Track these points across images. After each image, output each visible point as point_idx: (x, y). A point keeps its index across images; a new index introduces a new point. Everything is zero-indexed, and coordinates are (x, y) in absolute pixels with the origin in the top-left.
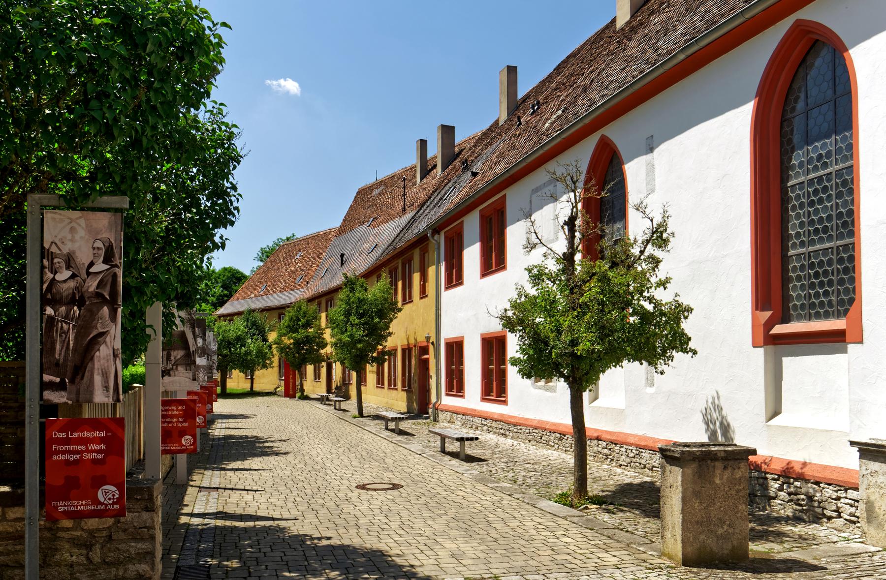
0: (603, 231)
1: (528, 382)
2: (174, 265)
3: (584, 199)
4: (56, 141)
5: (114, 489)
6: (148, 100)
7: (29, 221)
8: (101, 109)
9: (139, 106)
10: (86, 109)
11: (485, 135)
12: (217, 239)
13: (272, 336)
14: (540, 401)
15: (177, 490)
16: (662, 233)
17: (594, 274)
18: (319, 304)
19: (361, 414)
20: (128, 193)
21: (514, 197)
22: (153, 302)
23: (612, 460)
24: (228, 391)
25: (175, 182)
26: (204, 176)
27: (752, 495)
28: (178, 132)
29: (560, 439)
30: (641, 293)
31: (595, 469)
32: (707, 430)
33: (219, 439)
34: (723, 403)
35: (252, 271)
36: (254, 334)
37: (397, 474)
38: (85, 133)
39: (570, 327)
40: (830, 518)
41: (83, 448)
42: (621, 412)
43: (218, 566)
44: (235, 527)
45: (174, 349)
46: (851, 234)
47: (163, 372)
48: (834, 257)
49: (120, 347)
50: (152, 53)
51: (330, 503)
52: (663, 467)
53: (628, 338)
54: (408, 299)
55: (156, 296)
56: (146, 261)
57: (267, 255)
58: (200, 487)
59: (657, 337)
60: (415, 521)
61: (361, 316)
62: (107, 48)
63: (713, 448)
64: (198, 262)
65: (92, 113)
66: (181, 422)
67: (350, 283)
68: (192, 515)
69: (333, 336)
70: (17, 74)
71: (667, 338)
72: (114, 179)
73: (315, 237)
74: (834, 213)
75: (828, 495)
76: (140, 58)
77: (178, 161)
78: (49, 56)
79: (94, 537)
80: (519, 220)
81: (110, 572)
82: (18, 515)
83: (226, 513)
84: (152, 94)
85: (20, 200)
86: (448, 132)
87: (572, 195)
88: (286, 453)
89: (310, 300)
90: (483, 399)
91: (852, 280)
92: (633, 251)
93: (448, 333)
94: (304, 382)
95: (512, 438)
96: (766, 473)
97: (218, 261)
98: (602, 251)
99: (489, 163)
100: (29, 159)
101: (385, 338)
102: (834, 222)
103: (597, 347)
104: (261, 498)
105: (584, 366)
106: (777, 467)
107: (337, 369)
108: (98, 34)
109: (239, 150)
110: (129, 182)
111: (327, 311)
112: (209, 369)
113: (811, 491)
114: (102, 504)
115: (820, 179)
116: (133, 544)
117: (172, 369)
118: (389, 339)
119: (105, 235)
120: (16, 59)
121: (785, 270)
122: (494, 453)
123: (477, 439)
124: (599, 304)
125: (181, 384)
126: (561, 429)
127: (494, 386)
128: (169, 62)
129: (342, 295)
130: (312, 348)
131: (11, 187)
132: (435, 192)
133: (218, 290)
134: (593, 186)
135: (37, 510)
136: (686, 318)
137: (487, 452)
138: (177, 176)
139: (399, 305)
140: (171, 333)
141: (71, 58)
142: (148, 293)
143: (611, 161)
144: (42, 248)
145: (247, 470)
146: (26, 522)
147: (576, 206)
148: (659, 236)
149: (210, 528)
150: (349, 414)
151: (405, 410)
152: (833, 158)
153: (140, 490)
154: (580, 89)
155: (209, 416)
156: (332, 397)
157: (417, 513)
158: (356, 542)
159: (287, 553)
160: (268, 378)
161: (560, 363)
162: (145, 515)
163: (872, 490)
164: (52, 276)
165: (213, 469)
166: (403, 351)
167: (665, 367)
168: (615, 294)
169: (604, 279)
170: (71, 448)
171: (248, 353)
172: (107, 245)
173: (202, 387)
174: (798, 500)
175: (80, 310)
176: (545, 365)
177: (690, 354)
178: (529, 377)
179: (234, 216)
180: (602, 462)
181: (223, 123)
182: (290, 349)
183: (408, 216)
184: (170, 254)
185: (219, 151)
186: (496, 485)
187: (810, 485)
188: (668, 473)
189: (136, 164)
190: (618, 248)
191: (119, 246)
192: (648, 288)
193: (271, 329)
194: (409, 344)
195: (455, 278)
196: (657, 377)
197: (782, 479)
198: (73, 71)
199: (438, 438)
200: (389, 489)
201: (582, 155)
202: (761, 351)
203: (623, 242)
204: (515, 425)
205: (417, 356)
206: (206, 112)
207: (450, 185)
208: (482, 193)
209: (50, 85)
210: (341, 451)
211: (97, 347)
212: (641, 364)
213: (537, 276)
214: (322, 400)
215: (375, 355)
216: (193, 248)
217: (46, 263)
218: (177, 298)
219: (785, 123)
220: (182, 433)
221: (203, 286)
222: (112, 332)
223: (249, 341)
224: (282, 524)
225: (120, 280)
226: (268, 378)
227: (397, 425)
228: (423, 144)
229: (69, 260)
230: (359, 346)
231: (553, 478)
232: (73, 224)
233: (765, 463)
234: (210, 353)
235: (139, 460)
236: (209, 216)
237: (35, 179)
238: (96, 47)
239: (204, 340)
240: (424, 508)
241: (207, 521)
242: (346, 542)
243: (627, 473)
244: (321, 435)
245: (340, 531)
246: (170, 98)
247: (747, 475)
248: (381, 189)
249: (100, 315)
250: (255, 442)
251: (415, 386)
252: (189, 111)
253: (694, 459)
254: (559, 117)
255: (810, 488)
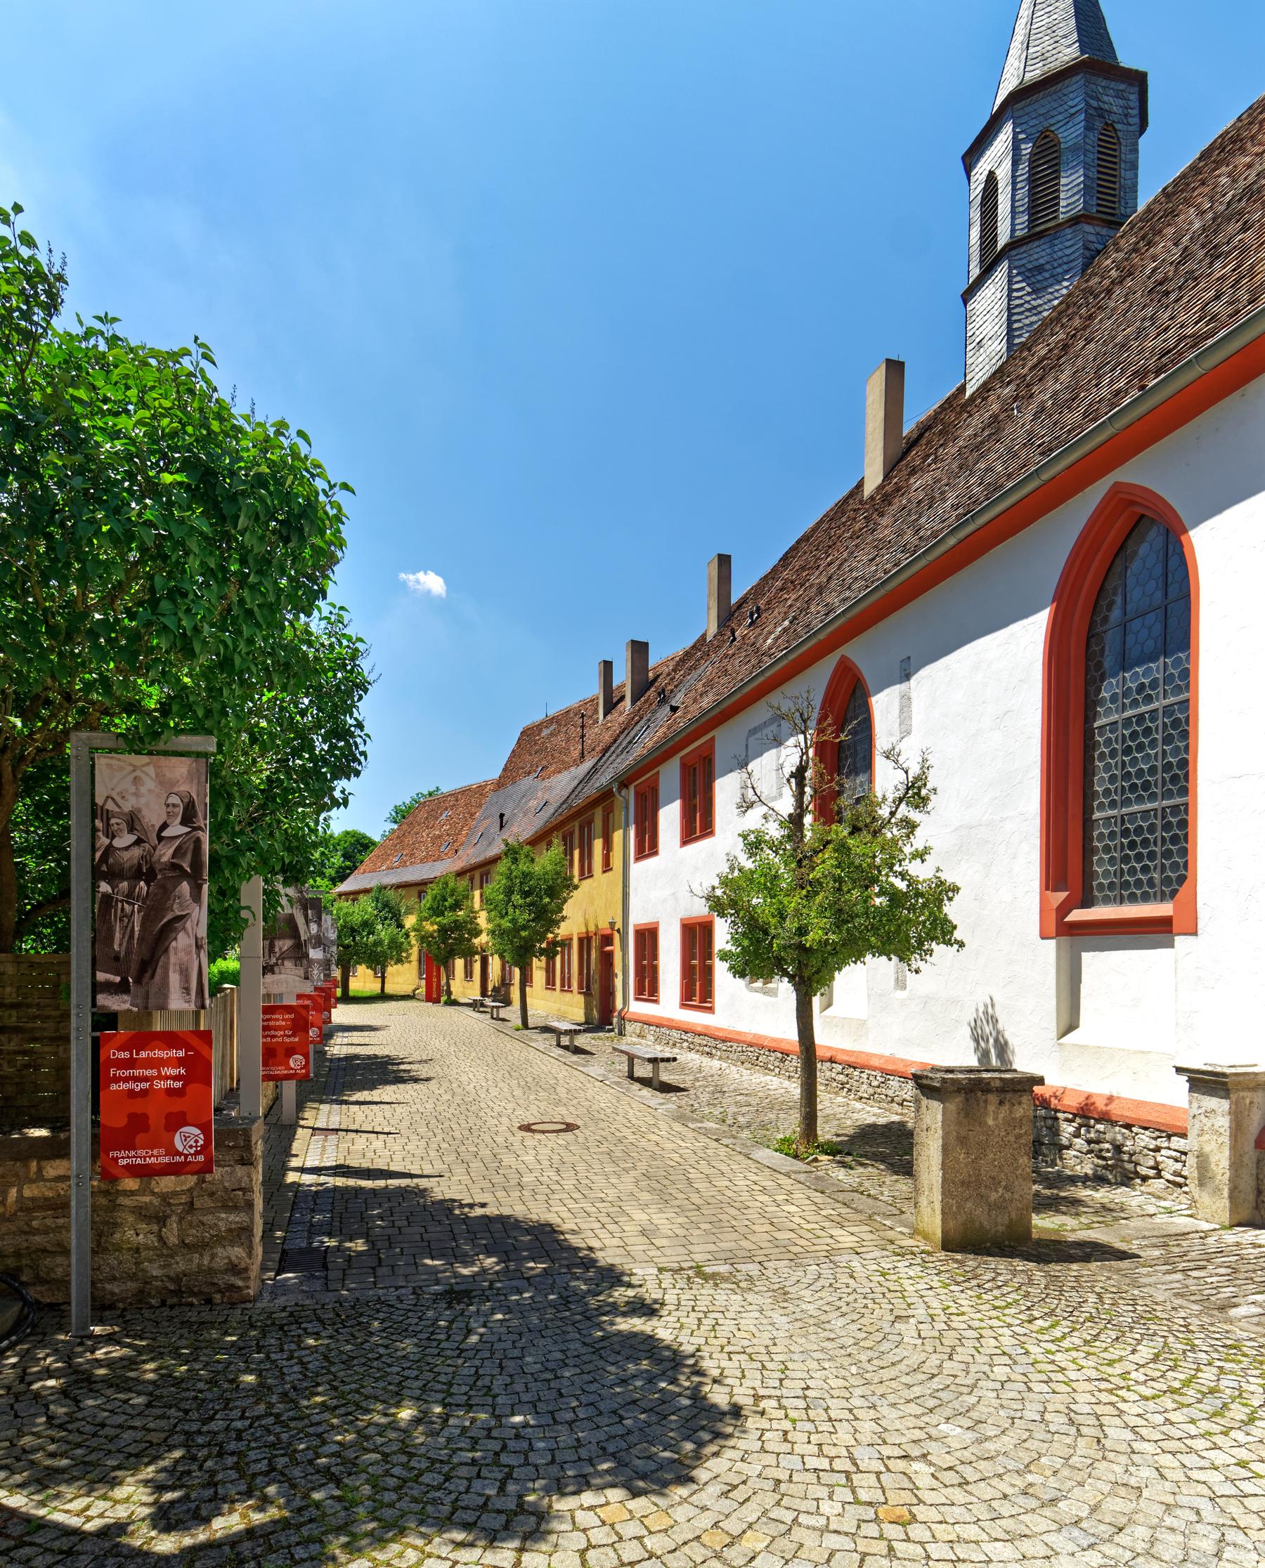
0: (842, 785)
1: (740, 983)
2: (279, 828)
3: (817, 743)
4: (112, 659)
5: (197, 1131)
6: (242, 601)
7: (73, 769)
8: (176, 614)
9: (229, 610)
10: (153, 613)
11: (688, 655)
12: (337, 794)
13: (410, 921)
14: (756, 1008)
15: (283, 1133)
16: (919, 789)
17: (828, 842)
18: (472, 879)
19: (525, 1025)
20: (215, 732)
21: (726, 740)
22: (251, 876)
23: (850, 1090)
24: (351, 994)
25: (280, 717)
26: (319, 709)
27: (1037, 1143)
28: (284, 648)
29: (782, 1061)
30: (891, 868)
31: (827, 1104)
32: (976, 1049)
33: (339, 1059)
34: (999, 1013)
35: (383, 836)
36: (386, 918)
37: (572, 1109)
38: (153, 648)
39: (796, 910)
40: (1145, 1179)
41: (154, 1072)
42: (862, 1023)
43: (338, 1248)
44: (361, 1188)
45: (280, 938)
46: (1184, 791)
47: (264, 968)
48: (1158, 822)
49: (205, 935)
50: (246, 530)
51: (485, 1152)
52: (917, 1101)
53: (873, 925)
54: (586, 873)
55: (254, 868)
56: (240, 822)
57: (402, 815)
58: (313, 1129)
59: (911, 924)
60: (594, 1178)
61: (526, 894)
62: (182, 521)
63: (985, 1075)
64: (312, 824)
65: (162, 619)
66: (289, 1036)
67: (512, 853)
68: (303, 1170)
69: (489, 920)
70: (51, 560)
71: (924, 926)
72: (195, 712)
73: (465, 792)
74: (1159, 764)
75: (1143, 1144)
76: (229, 538)
77: (284, 688)
78: (98, 532)
79: (169, 1204)
80: (731, 771)
81: (191, 1260)
82: (61, 1172)
83: (348, 1167)
84: (246, 593)
85: (59, 741)
86: (639, 650)
87: (801, 737)
88: (428, 1079)
89: (460, 874)
90: (683, 1006)
91: (1184, 852)
92: (880, 812)
93: (638, 917)
94: (451, 982)
95: (720, 1058)
96: (1057, 1111)
97: (339, 823)
98: (839, 812)
99: (692, 694)
100: (71, 683)
101: (556, 923)
102: (1159, 776)
103: (833, 937)
104: (395, 1144)
105: (815, 962)
106: (1072, 1102)
107: (495, 964)
108: (169, 500)
109: (366, 674)
110: (216, 716)
111: (481, 887)
112: (326, 965)
113: (1119, 1137)
114: (180, 1154)
115: (1141, 718)
116: (223, 1215)
117: (276, 964)
118: (562, 924)
119: (183, 788)
120: (49, 537)
121: (1087, 838)
122: (697, 1080)
123: (675, 1059)
124: (835, 881)
125: (289, 984)
126: (784, 1046)
127: (698, 988)
128: (271, 544)
129: (502, 867)
130: (462, 936)
131: (46, 722)
132: (622, 732)
133: (337, 860)
134: (829, 725)
135: (87, 1165)
136: (950, 899)
137: (687, 1078)
138: (282, 709)
139: (576, 880)
140: (274, 916)
141: (131, 537)
142: (244, 865)
143: (854, 691)
144: (93, 804)
145: (376, 1103)
146: (73, 1182)
147: (807, 753)
148: (916, 793)
149: (327, 1190)
150: (509, 1024)
151: (582, 1020)
152: (1161, 689)
153: (232, 1134)
154: (814, 589)
155: (325, 1028)
156: (488, 1002)
157: (597, 1166)
158: (519, 1211)
159: (430, 1229)
160: (404, 976)
161: (783, 958)
162: (240, 1171)
163: (1206, 1137)
164: (107, 841)
165: (332, 1102)
166: (581, 940)
167: (921, 964)
168: (856, 867)
169: (842, 848)
170: (137, 1072)
171: (378, 943)
172: (186, 800)
173: (316, 989)
174: (1101, 1150)
175: (148, 886)
176: (764, 960)
177: (956, 946)
178: (743, 975)
179: (360, 763)
180: (836, 1093)
181: (344, 635)
182: (433, 938)
183: (588, 765)
184: (273, 813)
185: (339, 675)
186: (700, 1125)
187: (1117, 1129)
188: (924, 1109)
189: (226, 692)
190: (861, 808)
191: (203, 801)
192: (900, 861)
193: (409, 911)
194: (587, 932)
195: (648, 846)
196: (911, 977)
197: (1078, 1120)
198: (133, 556)
199: (625, 1058)
200: (561, 1131)
201: (814, 684)
202: (1052, 944)
203: (866, 799)
204: (724, 1041)
205: (599, 946)
206: (320, 619)
207: (642, 723)
208: (683, 734)
209: (101, 577)
210: (499, 1076)
211: (173, 935)
212: (890, 959)
213: (754, 844)
214: (474, 1005)
215: (544, 945)
216: (305, 806)
217: (98, 824)
218: (283, 871)
219: (1093, 640)
220: (290, 1051)
221: (317, 855)
222: (195, 915)
223: (380, 927)
224: (423, 1183)
225: (206, 847)
226: (404, 976)
227: (572, 1040)
228: (607, 666)
229: (133, 822)
230: (523, 934)
231: (773, 1116)
232: (138, 773)
233: (1056, 1097)
234: (327, 943)
235: (231, 1090)
236: (326, 763)
237: (82, 711)
238: (167, 519)
239: (319, 925)
240: (606, 1158)
241: (323, 1179)
242: (506, 1211)
243: (869, 1109)
244: (474, 1054)
245: (498, 1194)
246: (271, 599)
247: (1031, 1113)
248: (553, 727)
249: (177, 892)
250: (387, 1063)
251: (596, 987)
252: (298, 619)
253: (959, 1091)
254: (785, 630)
255: (1118, 1133)
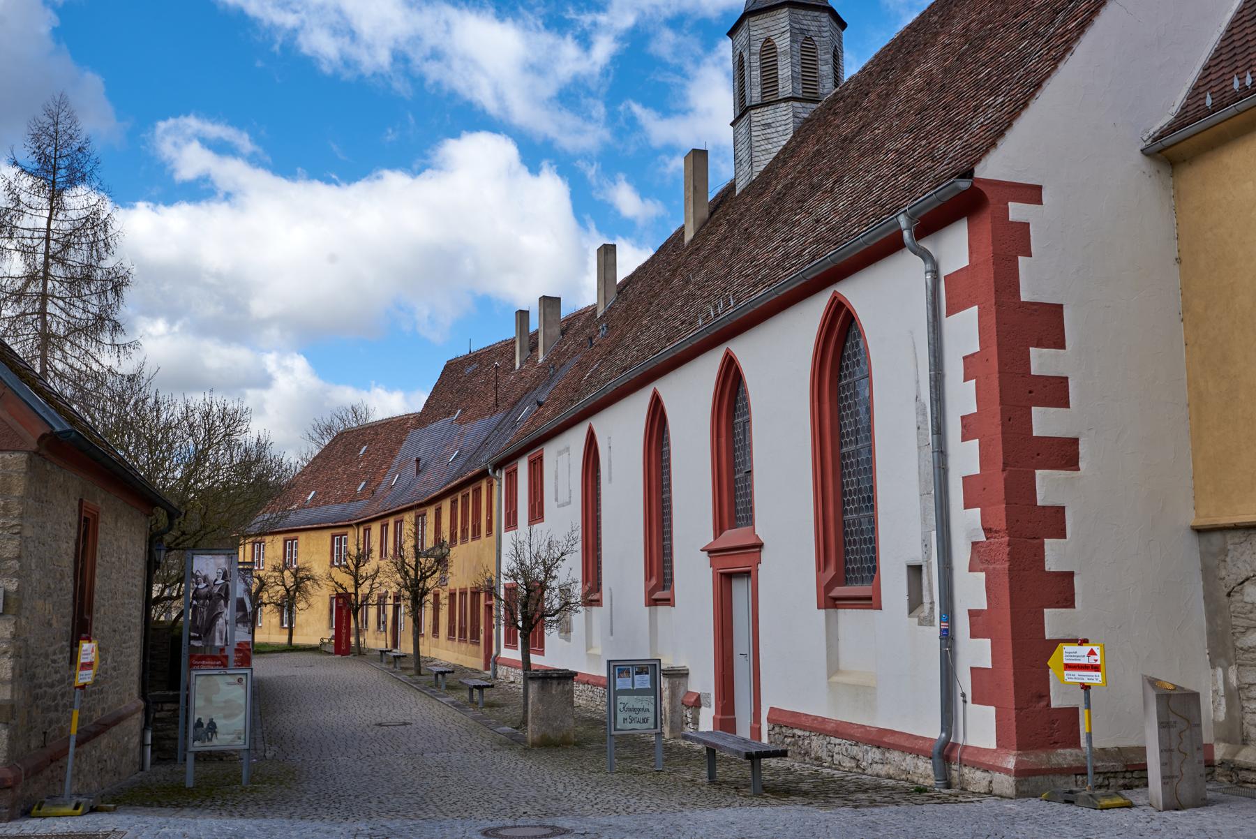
200: (502, 828)
202: (823, 611)
248: (475, 366)
